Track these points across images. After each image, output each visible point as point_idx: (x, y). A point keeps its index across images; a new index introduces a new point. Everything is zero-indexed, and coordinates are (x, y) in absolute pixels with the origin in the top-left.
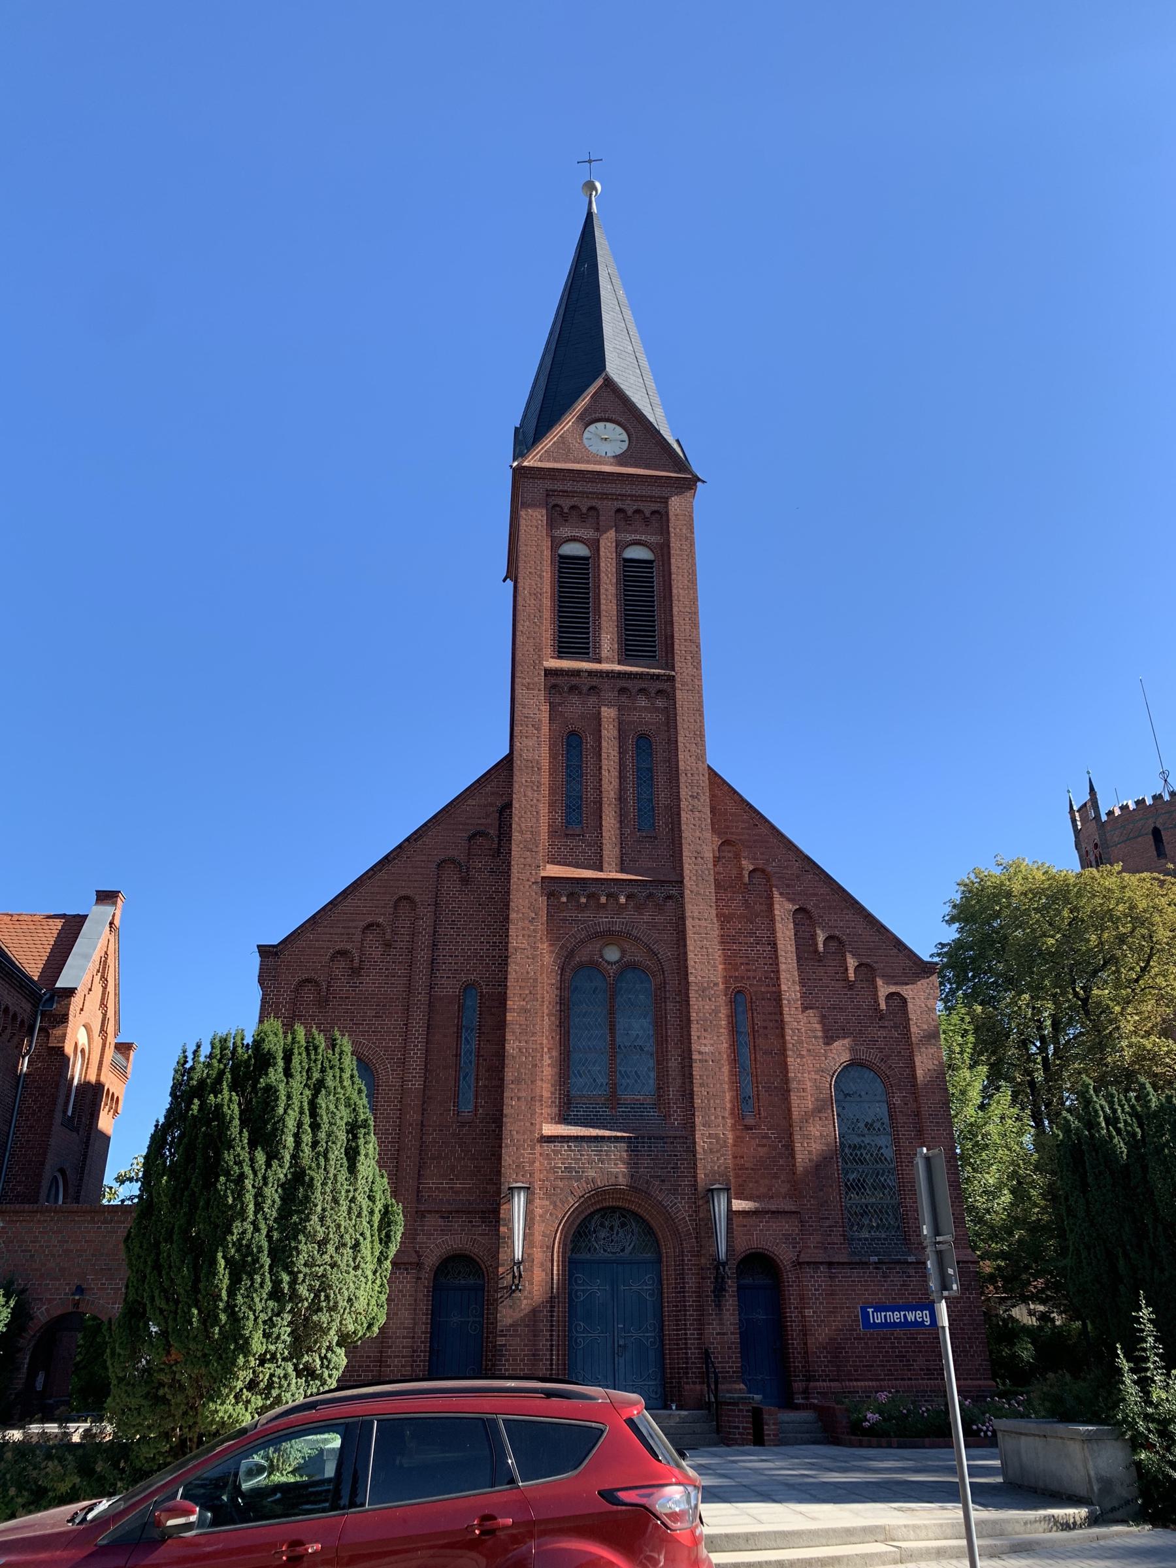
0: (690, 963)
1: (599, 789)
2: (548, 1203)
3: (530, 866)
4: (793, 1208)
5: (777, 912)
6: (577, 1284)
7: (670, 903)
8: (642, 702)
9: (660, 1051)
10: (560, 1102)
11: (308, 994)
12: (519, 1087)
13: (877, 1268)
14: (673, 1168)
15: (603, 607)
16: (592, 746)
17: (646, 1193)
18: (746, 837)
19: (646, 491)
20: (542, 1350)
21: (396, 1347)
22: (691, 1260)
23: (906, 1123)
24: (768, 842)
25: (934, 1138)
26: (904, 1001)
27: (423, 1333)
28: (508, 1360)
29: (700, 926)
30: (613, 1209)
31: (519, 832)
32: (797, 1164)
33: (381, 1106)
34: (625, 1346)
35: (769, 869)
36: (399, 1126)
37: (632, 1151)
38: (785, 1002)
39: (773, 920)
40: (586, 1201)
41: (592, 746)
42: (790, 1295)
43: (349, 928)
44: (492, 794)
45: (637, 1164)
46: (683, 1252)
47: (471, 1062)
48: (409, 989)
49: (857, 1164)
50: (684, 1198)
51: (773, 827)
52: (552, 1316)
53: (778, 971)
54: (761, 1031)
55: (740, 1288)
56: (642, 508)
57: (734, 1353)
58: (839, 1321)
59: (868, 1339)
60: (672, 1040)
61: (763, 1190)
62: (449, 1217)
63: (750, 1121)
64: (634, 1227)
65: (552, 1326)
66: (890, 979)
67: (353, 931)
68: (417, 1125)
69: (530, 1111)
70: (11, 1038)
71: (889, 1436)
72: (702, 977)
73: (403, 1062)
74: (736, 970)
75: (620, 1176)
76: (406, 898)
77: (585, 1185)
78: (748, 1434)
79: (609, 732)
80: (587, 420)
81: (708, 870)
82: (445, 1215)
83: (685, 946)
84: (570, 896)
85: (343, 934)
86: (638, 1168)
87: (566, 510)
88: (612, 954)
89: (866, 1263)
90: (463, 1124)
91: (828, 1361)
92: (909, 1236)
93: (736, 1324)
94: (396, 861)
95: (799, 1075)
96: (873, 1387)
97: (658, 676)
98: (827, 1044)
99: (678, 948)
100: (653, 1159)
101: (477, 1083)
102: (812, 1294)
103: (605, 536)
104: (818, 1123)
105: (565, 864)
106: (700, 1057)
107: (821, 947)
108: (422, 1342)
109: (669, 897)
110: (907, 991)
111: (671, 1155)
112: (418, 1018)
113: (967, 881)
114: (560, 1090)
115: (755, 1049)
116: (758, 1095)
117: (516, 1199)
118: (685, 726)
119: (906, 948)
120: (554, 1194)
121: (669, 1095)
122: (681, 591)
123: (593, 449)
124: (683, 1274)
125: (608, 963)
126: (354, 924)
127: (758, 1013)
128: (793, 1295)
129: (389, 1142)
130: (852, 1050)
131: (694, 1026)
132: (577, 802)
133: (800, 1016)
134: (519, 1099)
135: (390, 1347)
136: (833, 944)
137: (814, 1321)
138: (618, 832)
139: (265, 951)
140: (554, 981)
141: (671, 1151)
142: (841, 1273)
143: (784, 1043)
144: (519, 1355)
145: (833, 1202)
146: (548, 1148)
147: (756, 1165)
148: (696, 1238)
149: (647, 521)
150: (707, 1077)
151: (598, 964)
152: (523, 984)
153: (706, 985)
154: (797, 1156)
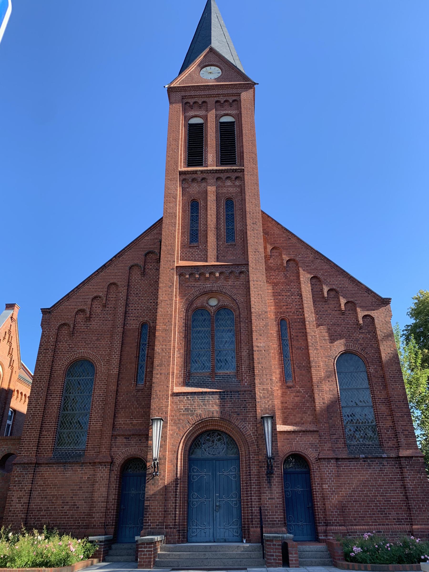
0: (252, 303)
1: (206, 225)
2: (175, 428)
3: (170, 261)
4: (315, 429)
5: (301, 279)
6: (194, 472)
7: (242, 275)
8: (229, 183)
9: (238, 348)
10: (184, 376)
11: (65, 331)
12: (161, 368)
13: (364, 461)
14: (244, 407)
15: (209, 143)
16: (203, 205)
17: (229, 421)
18: (285, 244)
19: (230, 91)
20: (170, 508)
21: (98, 507)
22: (254, 457)
23: (377, 382)
24: (296, 246)
25: (394, 389)
26: (373, 319)
28: (151, 514)
29: (257, 284)
30: (214, 431)
31: (165, 246)
32: (316, 405)
33: (98, 383)
34: (219, 506)
35: (297, 259)
37: (221, 399)
38: (307, 322)
39: (300, 284)
40: (197, 426)
41: (203, 205)
42: (314, 477)
43: (85, 299)
44: (157, 234)
45: (224, 406)
46: (249, 453)
47: (144, 360)
50: (250, 424)
51: (298, 239)
52: (176, 489)
53: (303, 308)
54: (295, 338)
55: (286, 473)
56: (228, 99)
57: (279, 510)
58: (344, 491)
59: (361, 501)
60: (244, 342)
61: (298, 420)
62: (129, 438)
63: (290, 384)
64: (225, 441)
65: (176, 495)
66: (364, 308)
67: (87, 300)
68: (114, 391)
69: (166, 380)
71: (366, 563)
72: (259, 309)
73: (108, 361)
74: (281, 308)
75: (215, 412)
76: (114, 284)
77: (195, 418)
78: (279, 560)
79: (211, 198)
80: (202, 66)
81: (262, 257)
82: (127, 437)
83: (250, 295)
84: (191, 274)
85: (81, 302)
86: (224, 408)
88: (213, 302)
89: (358, 458)
90: (138, 391)
91: (338, 515)
92: (382, 443)
93: (280, 493)
94: (109, 267)
95: (316, 359)
96: (365, 529)
97: (236, 170)
98: (332, 343)
99: (247, 297)
100: (232, 403)
101: (146, 370)
103: (210, 112)
104: (328, 384)
105: (189, 260)
106: (258, 349)
107: (326, 295)
108: (112, 505)
109: (241, 272)
110: (373, 313)
111: (242, 401)
112: (118, 339)
113: (417, 297)
114: (184, 369)
115: (292, 348)
116: (294, 370)
117: (156, 425)
118: (249, 191)
119: (372, 292)
120: (179, 423)
121: (242, 370)
122: (247, 131)
123: (205, 78)
124: (249, 465)
125: (211, 306)
126: (88, 297)
127: (293, 329)
128: (316, 476)
129: (100, 401)
130: (345, 345)
131: (254, 334)
132: (196, 232)
133: (315, 329)
134: (161, 374)
135: (95, 507)
136: (332, 294)
137: (329, 491)
138: (216, 243)
139: (44, 311)
140: (182, 316)
141: (243, 398)
142: (343, 464)
143: (307, 343)
144: (156, 511)
145: (338, 425)
146: (177, 399)
147: (294, 407)
150: (262, 358)
151: (205, 307)
152: (165, 317)
153: (260, 313)
154: (316, 401)
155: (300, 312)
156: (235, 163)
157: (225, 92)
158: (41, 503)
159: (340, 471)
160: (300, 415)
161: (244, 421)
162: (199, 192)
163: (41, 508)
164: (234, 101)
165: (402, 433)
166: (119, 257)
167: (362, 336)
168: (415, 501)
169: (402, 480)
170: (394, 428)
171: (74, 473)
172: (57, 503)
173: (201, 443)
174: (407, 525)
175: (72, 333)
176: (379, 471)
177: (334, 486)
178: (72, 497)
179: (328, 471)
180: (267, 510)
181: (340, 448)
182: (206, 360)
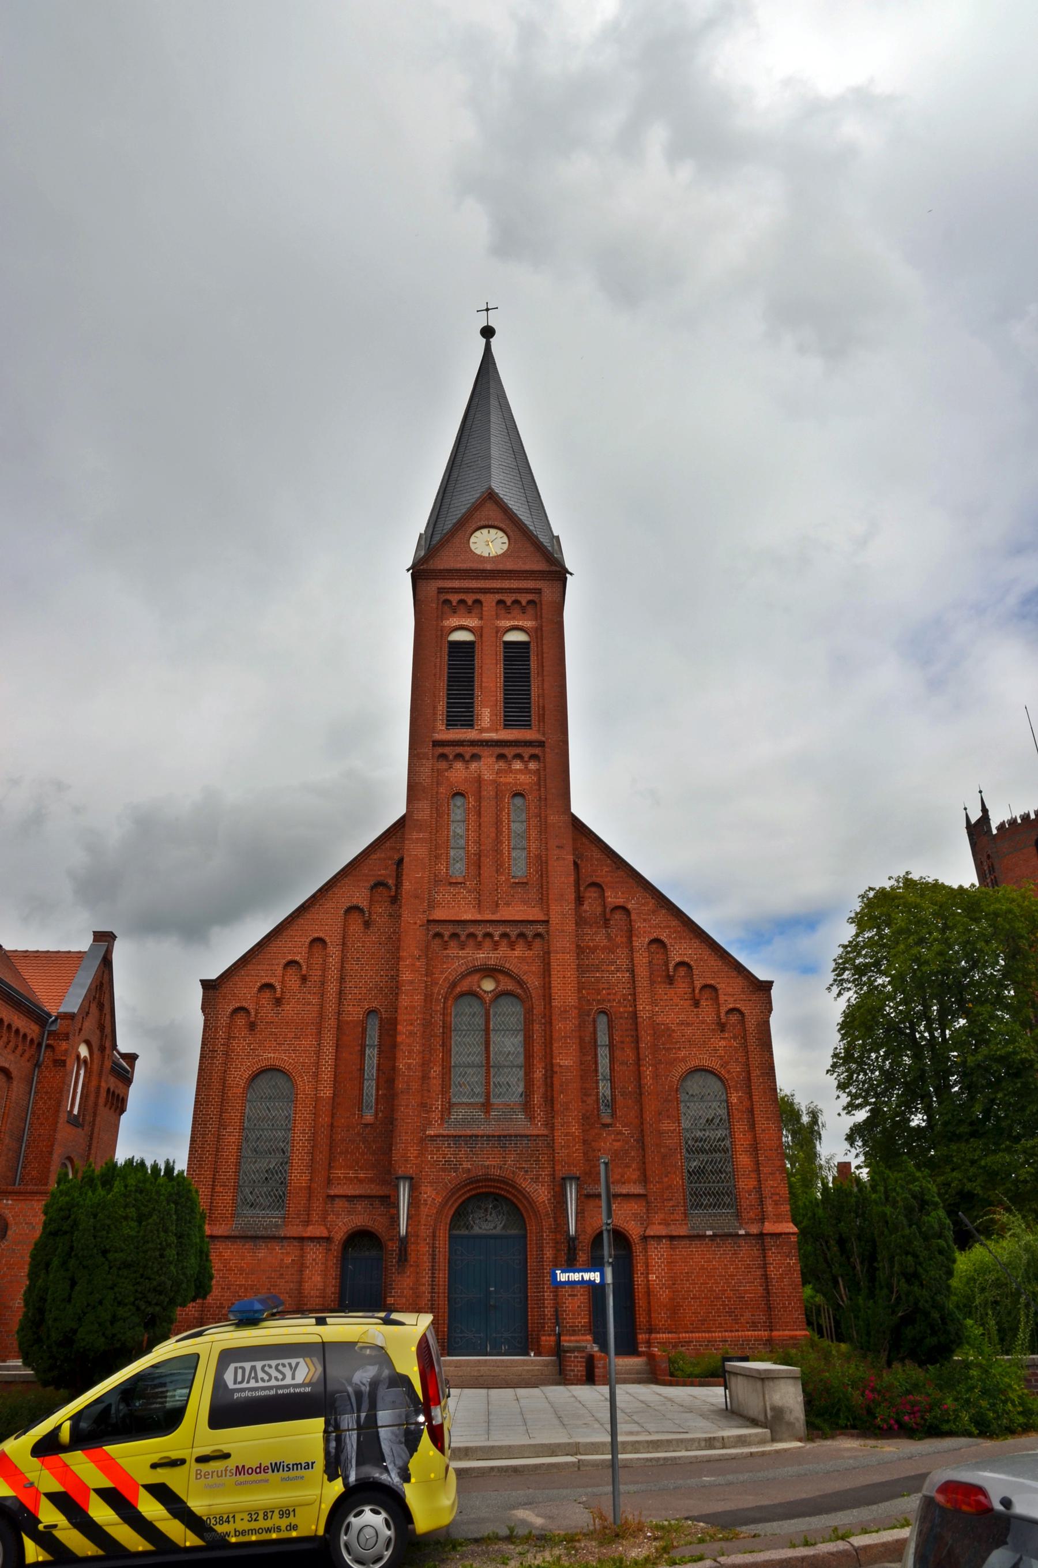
4: (642, 1191)
8: (518, 765)
13: (712, 1240)
27: (332, 1293)
30: (487, 1195)
35: (629, 906)
36: (314, 1127)
48: (321, 1014)
49: (698, 1153)
56: (519, 598)
73: (316, 1075)
74: (599, 994)
88: (488, 985)
102: (656, 1262)
108: (332, 1301)
109: (538, 935)
124: (542, 1247)
125: (485, 992)
139: (206, 984)
148: (554, 1217)
149: (524, 610)
155: (629, 1001)
156: (530, 725)
157: (515, 584)
158: (222, 1296)
159: (676, 1255)
161: (535, 1182)
162: (466, 780)
164: (530, 602)
167: (723, 1043)
168: (779, 1297)
170: (759, 1189)
174: (764, 1330)
175: (252, 1026)
176: (732, 1254)
178: (270, 1289)
179: (657, 1255)
180: (565, 1311)
181: (678, 1220)
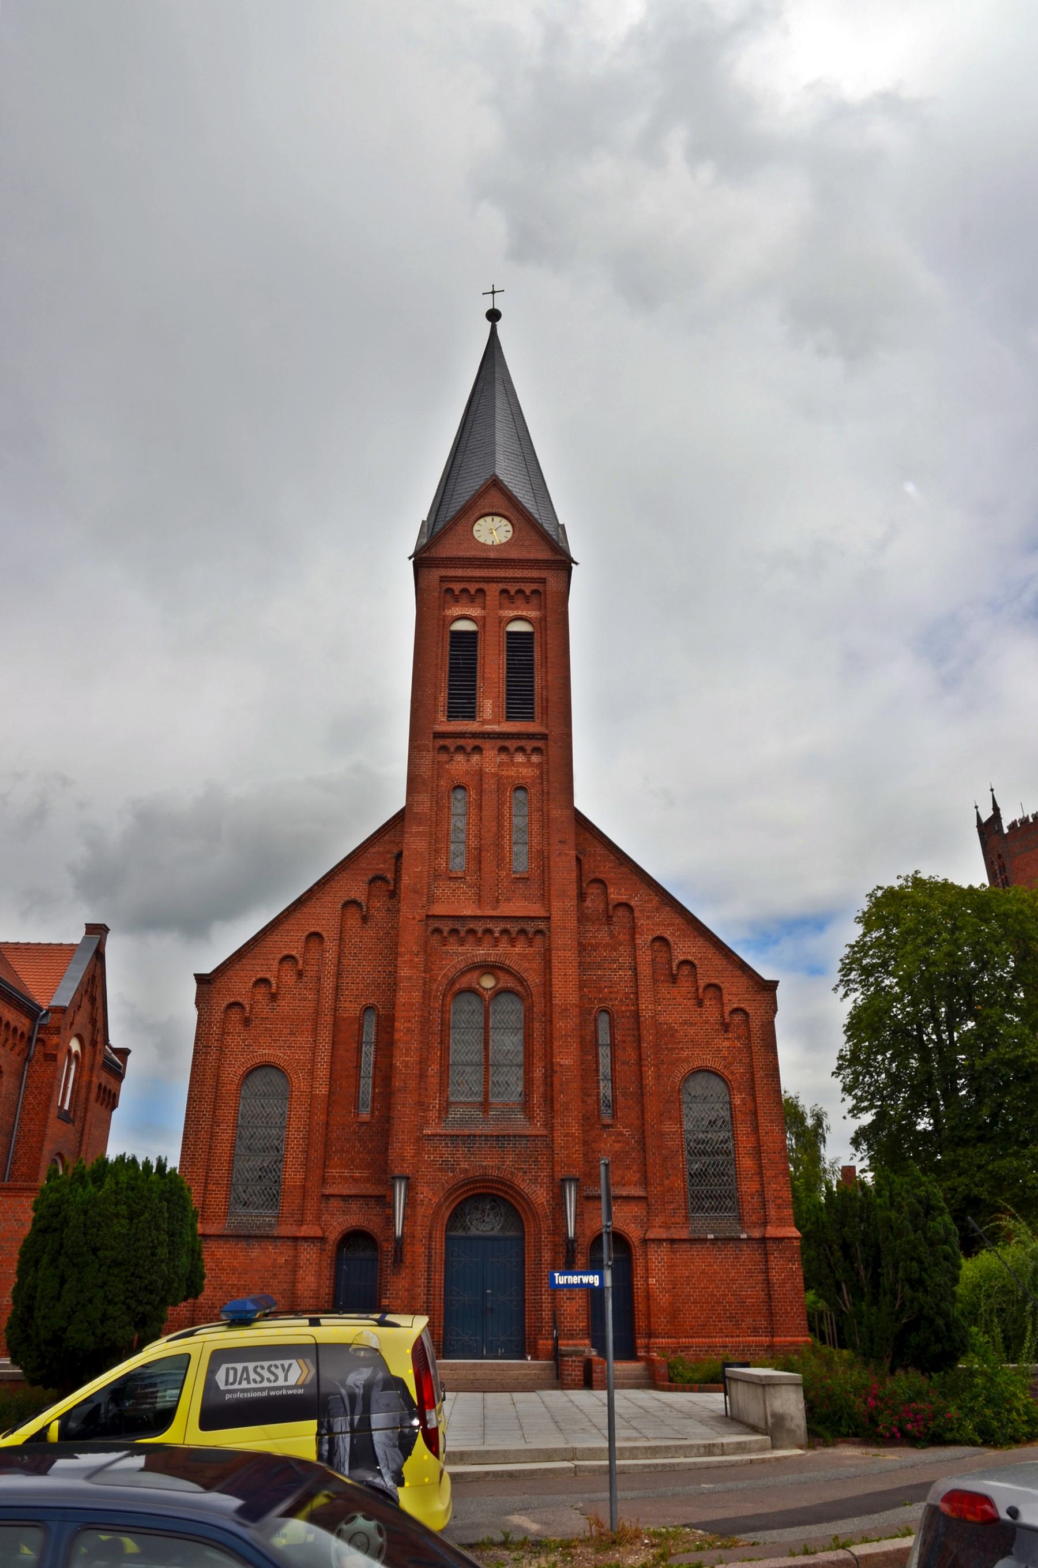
4: (642, 1194)
8: (520, 758)
16: (474, 799)
27: (326, 1294)
35: (632, 903)
36: (308, 1125)
41: (474, 799)
56: (523, 588)
57: (580, 1314)
70: (13, 1047)
74: (601, 992)
87: (457, 593)
109: (539, 932)
124: (540, 1249)
125: (485, 989)
149: (527, 599)
155: (631, 999)
157: (519, 573)
159: (677, 1259)
160: (620, 1172)
161: (534, 1183)
162: (467, 772)
163: (214, 1304)
164: (534, 592)
165: (773, 1201)
166: (323, 884)
167: (726, 1044)
169: (765, 1272)
170: (762, 1193)
171: (264, 1253)
172: (238, 1296)
173: (465, 1213)
174: (766, 1336)
177: (664, 1281)
180: (563, 1314)
181: (679, 1224)
182: (475, 1081)
